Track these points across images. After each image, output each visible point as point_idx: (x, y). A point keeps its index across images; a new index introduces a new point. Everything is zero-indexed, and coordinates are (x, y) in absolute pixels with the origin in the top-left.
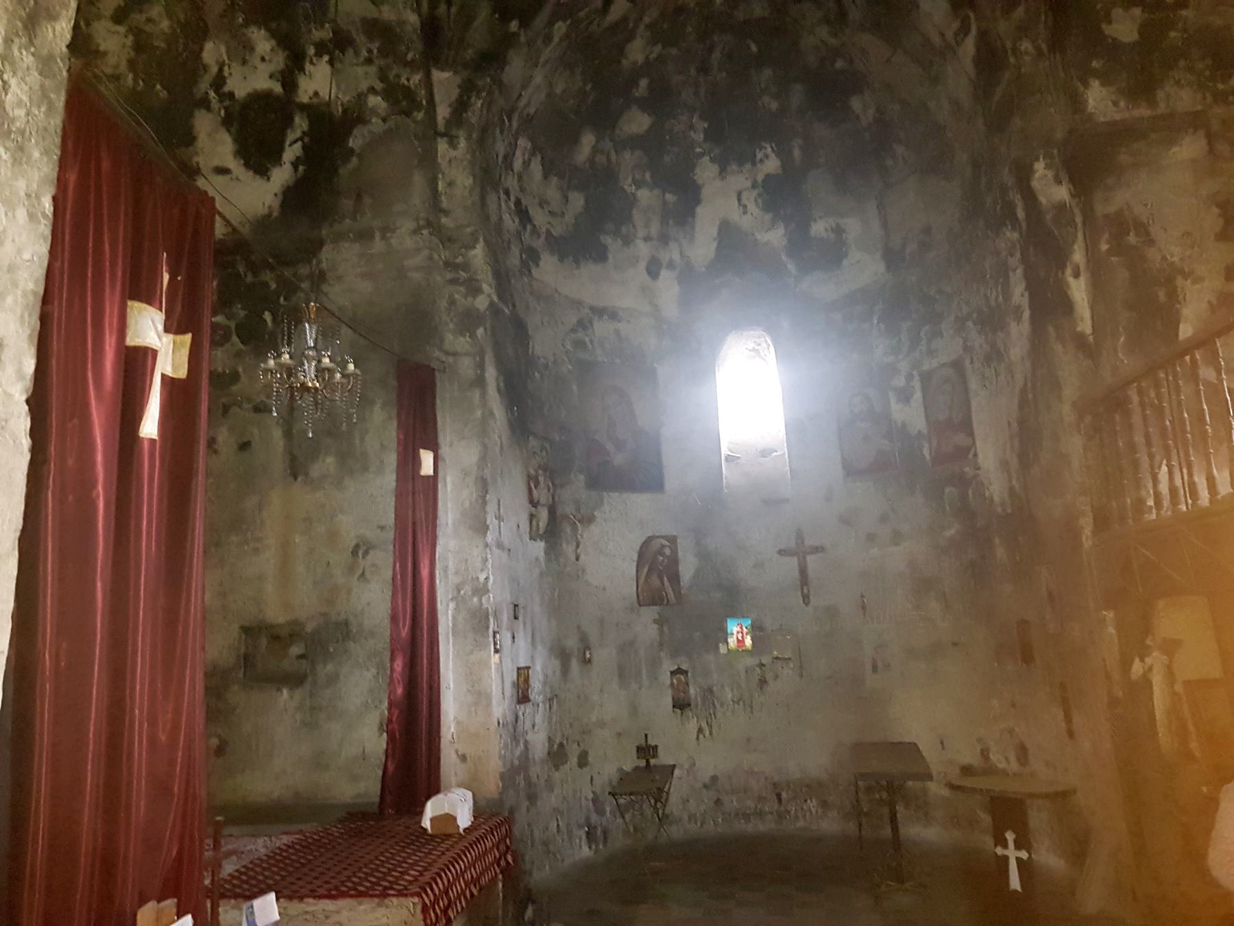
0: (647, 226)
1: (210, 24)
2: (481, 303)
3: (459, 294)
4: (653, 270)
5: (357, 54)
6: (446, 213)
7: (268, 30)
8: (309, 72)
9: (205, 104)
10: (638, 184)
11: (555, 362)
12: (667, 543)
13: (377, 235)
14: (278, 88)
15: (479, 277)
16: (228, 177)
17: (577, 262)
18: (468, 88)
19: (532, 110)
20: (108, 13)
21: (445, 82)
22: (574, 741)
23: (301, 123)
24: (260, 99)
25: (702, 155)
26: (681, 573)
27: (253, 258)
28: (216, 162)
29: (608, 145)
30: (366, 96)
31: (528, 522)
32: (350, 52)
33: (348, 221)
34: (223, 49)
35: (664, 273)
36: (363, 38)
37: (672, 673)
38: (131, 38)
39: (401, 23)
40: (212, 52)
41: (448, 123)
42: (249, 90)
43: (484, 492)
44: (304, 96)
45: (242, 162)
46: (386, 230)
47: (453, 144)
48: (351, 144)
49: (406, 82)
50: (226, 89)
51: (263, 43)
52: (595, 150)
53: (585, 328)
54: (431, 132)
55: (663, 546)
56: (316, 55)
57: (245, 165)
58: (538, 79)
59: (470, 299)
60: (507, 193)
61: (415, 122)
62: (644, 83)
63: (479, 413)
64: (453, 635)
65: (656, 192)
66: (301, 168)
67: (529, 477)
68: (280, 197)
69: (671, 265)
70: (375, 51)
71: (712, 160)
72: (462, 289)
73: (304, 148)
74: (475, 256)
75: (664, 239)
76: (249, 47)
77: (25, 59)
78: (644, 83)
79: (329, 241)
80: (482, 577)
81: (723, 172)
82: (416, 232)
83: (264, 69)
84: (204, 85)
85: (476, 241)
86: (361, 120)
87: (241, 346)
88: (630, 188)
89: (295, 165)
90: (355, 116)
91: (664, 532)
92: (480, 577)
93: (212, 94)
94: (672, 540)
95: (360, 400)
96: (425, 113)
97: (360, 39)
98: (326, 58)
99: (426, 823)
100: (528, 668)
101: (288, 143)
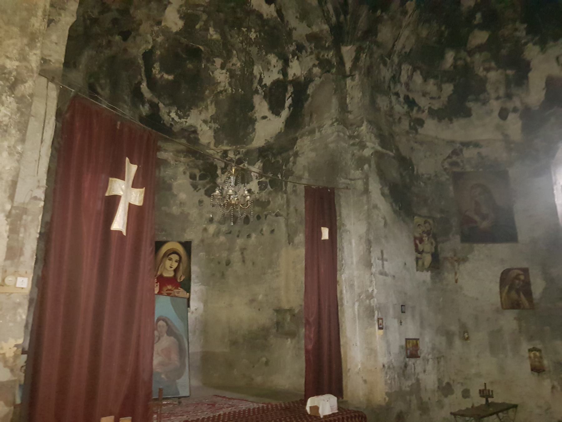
0: (497, 90)
1: (254, 59)
2: (367, 152)
3: (356, 150)
4: (503, 114)
5: (306, 52)
6: (350, 112)
7: (274, 53)
8: (291, 65)
9: (257, 92)
10: (488, 70)
11: (436, 176)
12: (522, 273)
13: (317, 131)
14: (281, 77)
15: (364, 140)
16: (267, 119)
17: (451, 120)
18: (359, 50)
19: (407, 50)
20: (219, 67)
21: (348, 52)
22: (459, 383)
23: (290, 89)
24: (276, 83)
25: (526, 44)
26: (533, 291)
27: (274, 151)
28: (263, 115)
29: (463, 54)
30: (312, 69)
31: (415, 263)
32: (304, 52)
33: (307, 127)
34: (260, 67)
35: (511, 117)
36: (308, 44)
37: (530, 350)
38: (228, 73)
39: (321, 31)
40: (257, 69)
41: (351, 70)
42: (272, 81)
43: (370, 246)
44: (290, 78)
45: (271, 112)
46: (320, 127)
47: (353, 80)
48: (308, 92)
49: (327, 57)
50: (263, 83)
51: (273, 59)
52: (455, 59)
53: (457, 154)
54: (345, 76)
55: (519, 275)
56: (292, 58)
57: (272, 113)
58: (406, 33)
59: (361, 151)
60: (397, 94)
61: (332, 74)
62: (478, 16)
63: (366, 207)
64: (358, 319)
65: (500, 71)
66: (291, 108)
67: (415, 238)
68: (284, 123)
69: (515, 110)
70: (313, 48)
71: (535, 44)
72: (357, 147)
73: (292, 99)
74: (362, 130)
75: (509, 96)
76: (269, 63)
77: (8, 100)
78: (478, 16)
79: (299, 138)
80: (370, 290)
81: (543, 50)
82: (332, 124)
83: (275, 70)
84: (256, 84)
85: (363, 122)
86: (311, 80)
87: (271, 189)
88: (481, 72)
89: (289, 108)
90: (309, 79)
91: (519, 266)
92: (369, 289)
93: (259, 87)
94: (526, 271)
95: (227, 207)
96: (336, 69)
97: (307, 44)
98: (296, 57)
99: (308, 409)
100: (417, 340)
101: (287, 99)
